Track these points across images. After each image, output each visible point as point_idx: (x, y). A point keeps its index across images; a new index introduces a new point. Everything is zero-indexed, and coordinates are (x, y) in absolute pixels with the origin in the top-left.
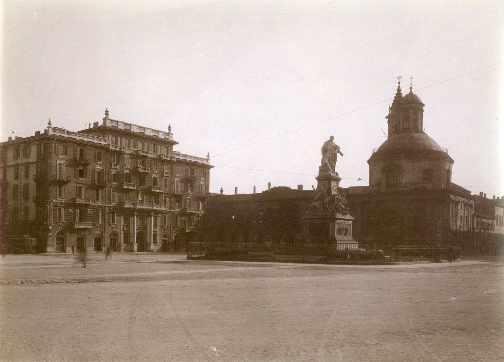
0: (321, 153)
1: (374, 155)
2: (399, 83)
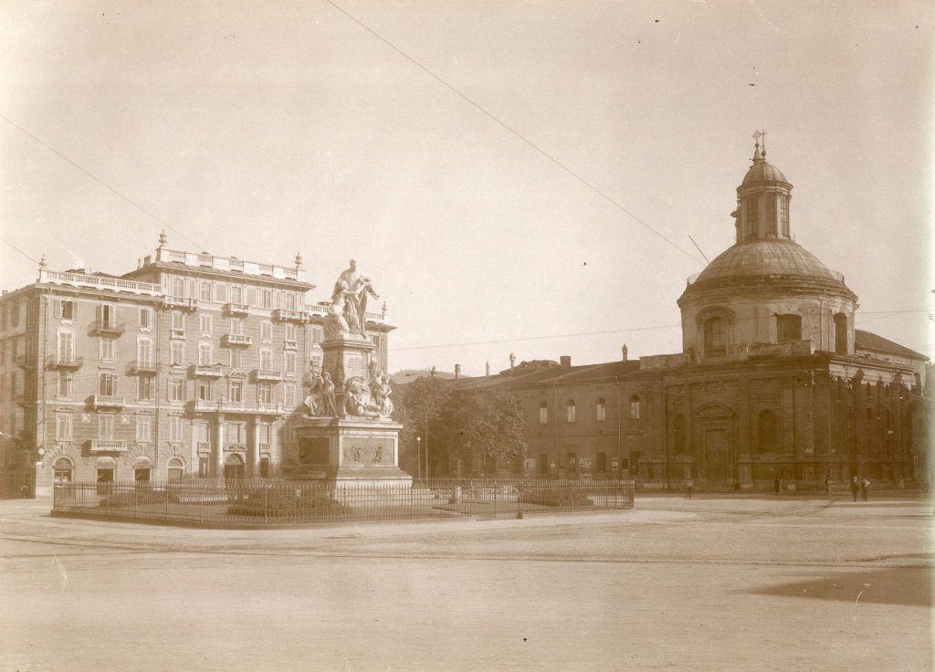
1: (691, 289)
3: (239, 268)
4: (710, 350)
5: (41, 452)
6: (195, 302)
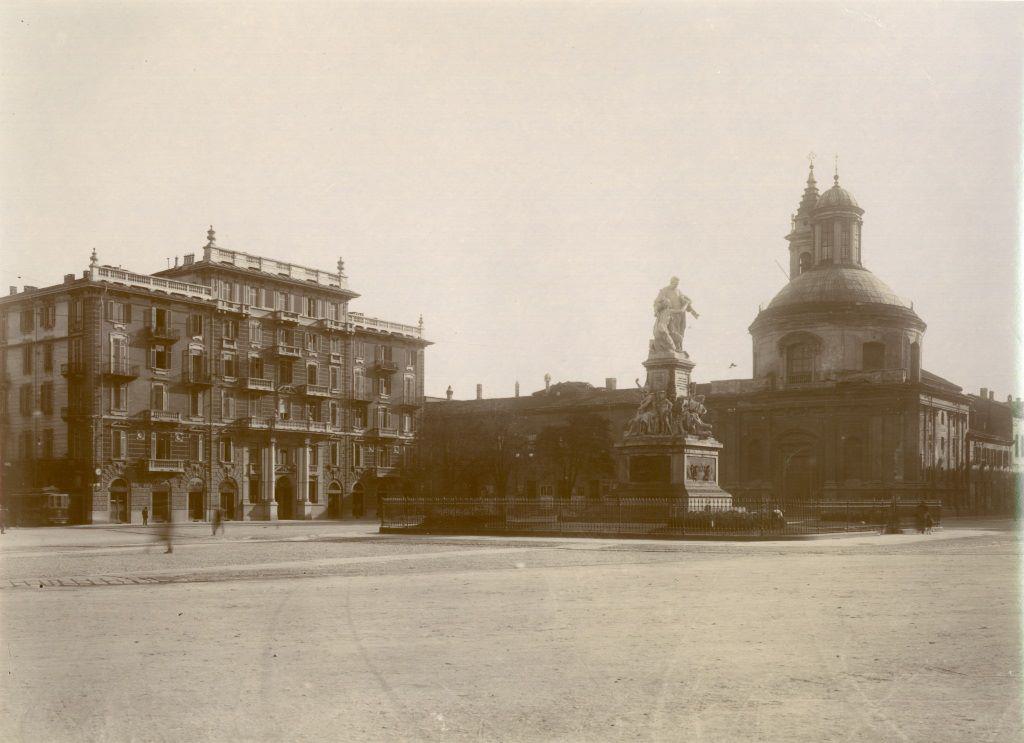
3: (286, 272)
4: (792, 379)
5: (98, 472)
6: (247, 307)
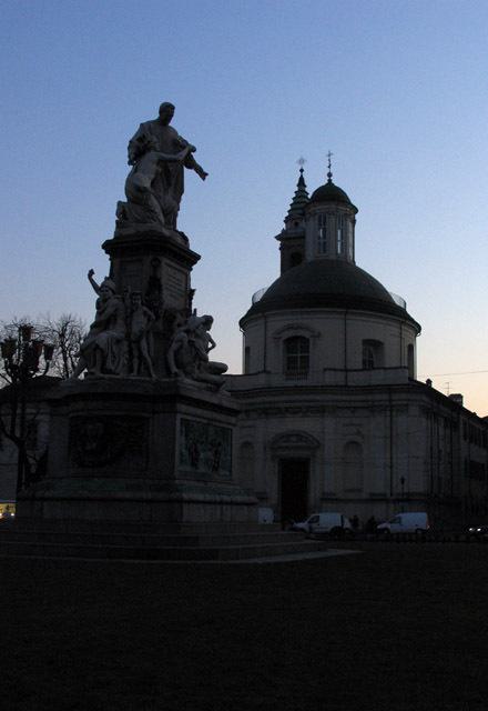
0: (124, 155)
2: (302, 171)
